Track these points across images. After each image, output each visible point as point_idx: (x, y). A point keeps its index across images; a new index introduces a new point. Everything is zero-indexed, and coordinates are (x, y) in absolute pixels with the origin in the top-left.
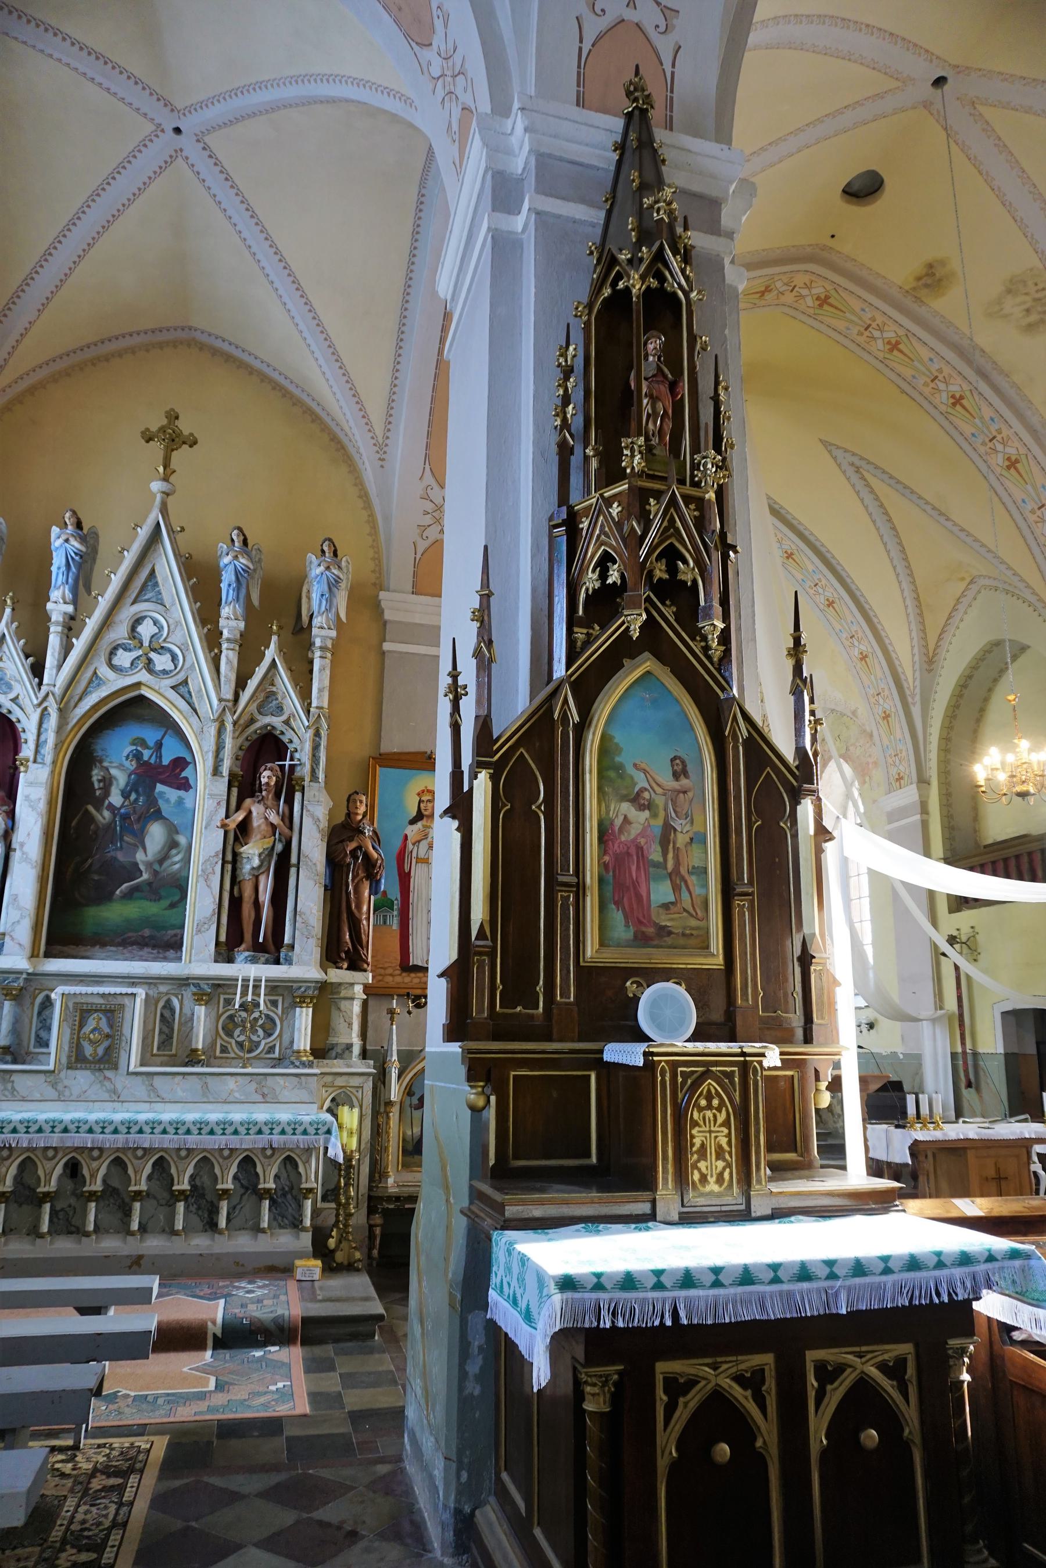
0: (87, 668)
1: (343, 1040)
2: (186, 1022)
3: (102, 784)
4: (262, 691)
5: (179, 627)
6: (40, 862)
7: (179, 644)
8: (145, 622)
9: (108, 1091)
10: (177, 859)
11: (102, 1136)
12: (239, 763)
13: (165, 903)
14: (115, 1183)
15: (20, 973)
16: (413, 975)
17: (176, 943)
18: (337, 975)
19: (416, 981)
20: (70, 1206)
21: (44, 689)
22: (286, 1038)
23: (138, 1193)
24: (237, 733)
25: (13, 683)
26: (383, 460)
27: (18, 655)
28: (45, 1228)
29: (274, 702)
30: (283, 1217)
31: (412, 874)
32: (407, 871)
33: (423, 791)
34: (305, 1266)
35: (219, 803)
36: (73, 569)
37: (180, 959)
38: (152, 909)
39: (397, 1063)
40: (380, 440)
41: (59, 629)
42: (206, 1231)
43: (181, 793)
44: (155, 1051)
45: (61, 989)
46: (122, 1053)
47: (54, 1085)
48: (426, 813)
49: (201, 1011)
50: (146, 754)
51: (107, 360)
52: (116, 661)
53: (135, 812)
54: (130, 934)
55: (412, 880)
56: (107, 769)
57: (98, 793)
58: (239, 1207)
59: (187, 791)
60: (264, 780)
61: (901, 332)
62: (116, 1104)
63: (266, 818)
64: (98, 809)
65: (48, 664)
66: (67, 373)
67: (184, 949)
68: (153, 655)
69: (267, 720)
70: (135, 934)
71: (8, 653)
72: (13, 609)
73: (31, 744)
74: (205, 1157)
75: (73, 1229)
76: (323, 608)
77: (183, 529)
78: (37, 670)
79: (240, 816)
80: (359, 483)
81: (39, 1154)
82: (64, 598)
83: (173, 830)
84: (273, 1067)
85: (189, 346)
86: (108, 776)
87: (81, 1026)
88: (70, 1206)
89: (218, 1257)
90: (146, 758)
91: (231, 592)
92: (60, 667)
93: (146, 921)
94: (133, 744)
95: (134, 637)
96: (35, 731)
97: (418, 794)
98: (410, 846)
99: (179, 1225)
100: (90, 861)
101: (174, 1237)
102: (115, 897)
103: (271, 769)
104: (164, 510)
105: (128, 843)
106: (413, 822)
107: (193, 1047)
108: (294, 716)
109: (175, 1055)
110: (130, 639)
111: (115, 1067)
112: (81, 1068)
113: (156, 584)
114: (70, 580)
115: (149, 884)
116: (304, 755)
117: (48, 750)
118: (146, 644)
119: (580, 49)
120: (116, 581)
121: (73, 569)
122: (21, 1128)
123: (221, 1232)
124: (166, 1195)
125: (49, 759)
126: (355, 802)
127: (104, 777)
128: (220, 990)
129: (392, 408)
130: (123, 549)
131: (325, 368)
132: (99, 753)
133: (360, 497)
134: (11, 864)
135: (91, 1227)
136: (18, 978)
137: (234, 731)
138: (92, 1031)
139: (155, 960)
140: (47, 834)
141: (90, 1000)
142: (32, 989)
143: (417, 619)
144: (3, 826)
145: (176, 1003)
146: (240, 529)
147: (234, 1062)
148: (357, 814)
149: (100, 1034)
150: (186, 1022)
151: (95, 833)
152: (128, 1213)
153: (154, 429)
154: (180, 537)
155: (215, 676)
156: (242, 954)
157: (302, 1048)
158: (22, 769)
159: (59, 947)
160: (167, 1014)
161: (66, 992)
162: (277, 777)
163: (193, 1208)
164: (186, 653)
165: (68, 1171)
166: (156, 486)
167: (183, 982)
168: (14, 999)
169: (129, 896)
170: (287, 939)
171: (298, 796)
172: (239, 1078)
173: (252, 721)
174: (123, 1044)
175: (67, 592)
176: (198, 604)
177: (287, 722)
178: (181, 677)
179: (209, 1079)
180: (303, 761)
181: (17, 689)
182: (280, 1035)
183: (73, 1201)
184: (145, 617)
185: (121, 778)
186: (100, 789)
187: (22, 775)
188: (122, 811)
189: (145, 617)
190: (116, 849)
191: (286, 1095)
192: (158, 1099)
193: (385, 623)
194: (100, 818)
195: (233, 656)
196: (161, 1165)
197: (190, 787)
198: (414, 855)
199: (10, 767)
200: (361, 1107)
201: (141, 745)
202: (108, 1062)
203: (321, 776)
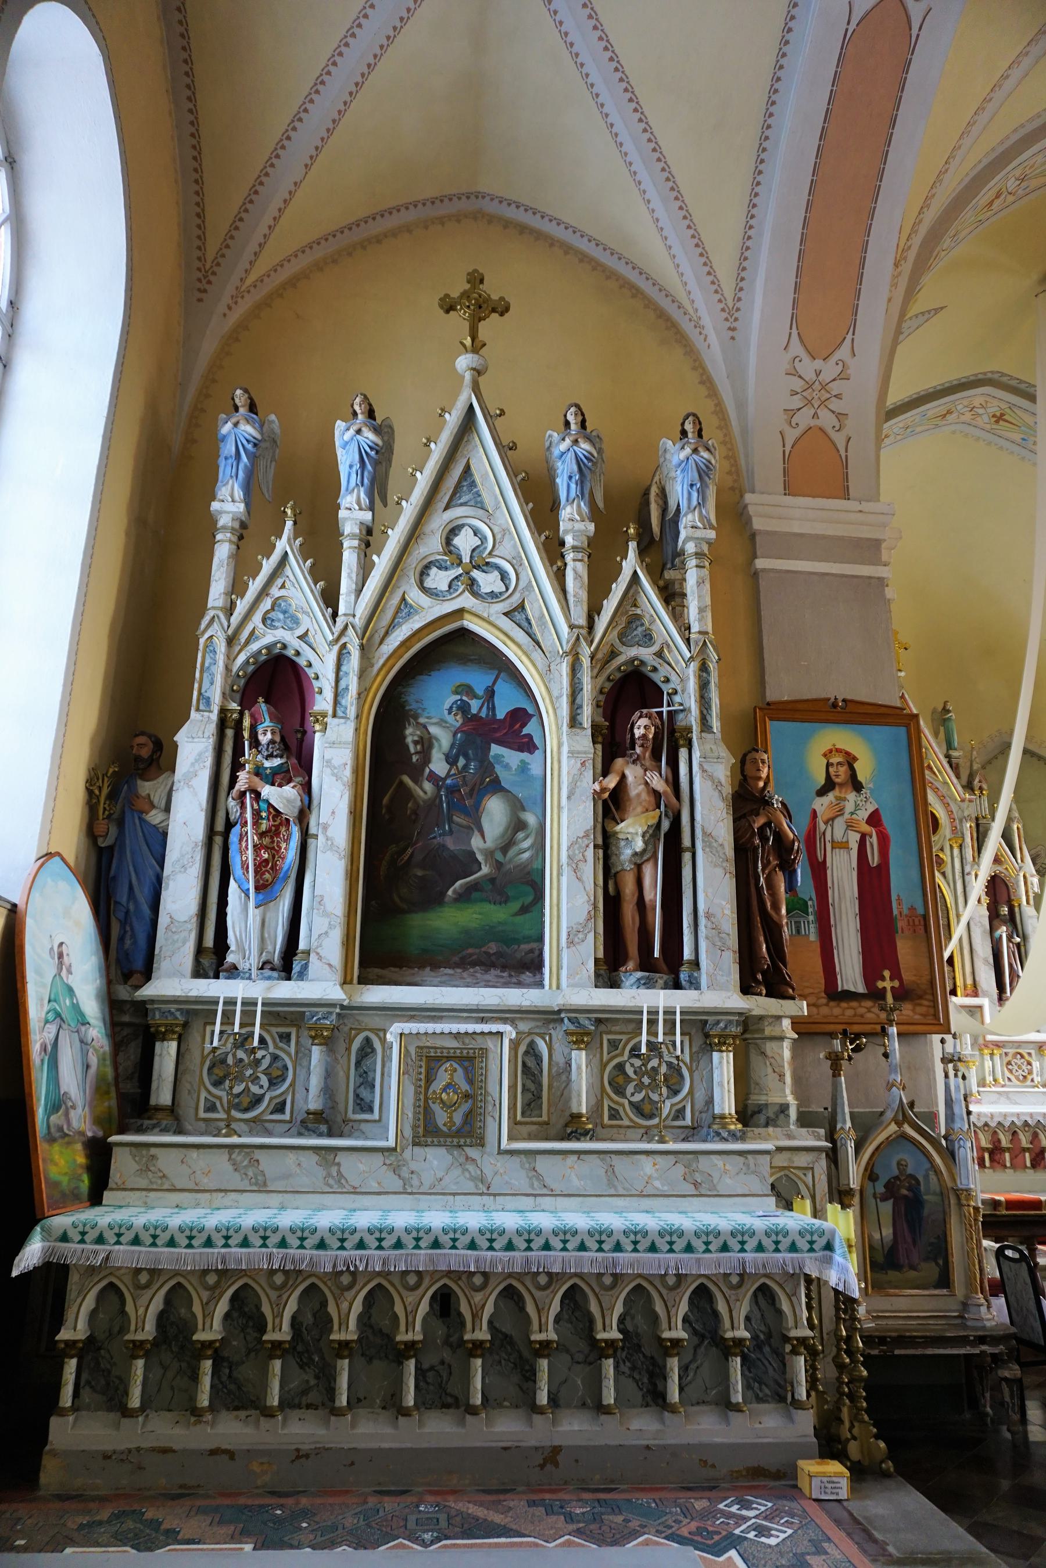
0: (391, 593)
1: (775, 1099)
2: (559, 1074)
3: (419, 747)
4: (622, 614)
5: (507, 536)
6: (348, 852)
7: (509, 558)
8: (463, 531)
9: (472, 1179)
10: (526, 844)
11: (490, 1253)
12: (600, 710)
13: (515, 906)
14: (507, 1327)
15: (333, 1005)
16: (844, 1005)
17: (532, 961)
18: (760, 1005)
19: (849, 1013)
20: (442, 1363)
21: (341, 621)
22: (700, 1095)
23: (546, 1344)
24: (596, 671)
25: (299, 615)
26: (733, 329)
27: (305, 578)
28: (410, 1400)
29: (640, 629)
30: (760, 1383)
31: (829, 864)
32: (820, 859)
33: (831, 751)
34: (824, 1474)
35: (583, 764)
36: (369, 467)
37: (540, 985)
38: (498, 914)
39: (852, 1132)
40: (730, 304)
41: (356, 543)
42: (647, 1405)
43: (524, 756)
44: (519, 1117)
45: (395, 1030)
46: (489, 1119)
47: (396, 1170)
48: (837, 780)
49: (580, 1058)
50: (475, 705)
51: (379, 242)
52: (429, 583)
53: (465, 784)
54: (470, 951)
55: (829, 872)
56: (425, 727)
57: (415, 758)
58: (693, 1366)
59: (531, 753)
60: (638, 733)
61: (1004, 406)
62: (485, 1198)
63: (647, 783)
64: (417, 781)
65: (343, 589)
66: (334, 260)
67: (546, 970)
68: (476, 574)
69: (633, 652)
70: (477, 951)
71: (292, 577)
72: (295, 523)
73: (329, 694)
74: (639, 1286)
75: (450, 1400)
76: (694, 502)
77: (502, 413)
78: (330, 599)
79: (611, 782)
80: (699, 365)
81: (396, 1281)
82: (358, 503)
83: (517, 806)
84: (685, 1140)
85: (475, 219)
86: (426, 736)
87: (429, 1080)
88: (442, 1363)
89: (674, 1452)
90: (474, 711)
91: (573, 486)
92: (359, 591)
93: (491, 933)
94: (456, 693)
95: (450, 552)
96: (331, 676)
97: (825, 755)
98: (822, 826)
99: (609, 1397)
100: (410, 851)
101: (603, 1417)
102: (447, 899)
103: (649, 716)
104: (476, 389)
105: (458, 824)
106: (822, 792)
107: (575, 1111)
108: (668, 646)
109: (547, 1123)
110: (445, 554)
111: (481, 1143)
112: (432, 1145)
113: (473, 484)
114: (366, 481)
115: (491, 880)
116: (690, 698)
117: (350, 700)
118: (466, 559)
119: (784, 452)
120: (423, 480)
121: (369, 467)
122: (371, 1241)
123: (672, 1409)
124: (583, 1345)
125: (352, 712)
126: (755, 761)
127: (422, 738)
128: (602, 1027)
129: (746, 259)
130: (429, 440)
131: (660, 213)
132: (413, 706)
133: (702, 382)
134: (311, 855)
135: (477, 1400)
136: (331, 1013)
137: (592, 668)
138: (444, 1090)
139: (506, 985)
140: (354, 813)
141: (439, 1043)
142: (346, 1029)
143: (796, 528)
144: (299, 803)
145: (542, 1046)
146: (577, 406)
147: (630, 1133)
148: (760, 778)
149: (455, 1092)
150: (559, 1074)
151: (415, 813)
152: (530, 1376)
153: (455, 294)
154: (499, 422)
155: (561, 596)
156: (631, 975)
157: (727, 1112)
158: (317, 727)
159: (377, 970)
160: (531, 1063)
161: (406, 1032)
162: (656, 727)
163: (625, 1368)
164: (520, 570)
165: (437, 1307)
166: (464, 362)
167: (550, 1017)
168: (325, 1044)
169: (465, 897)
170: (687, 954)
171: (683, 753)
172: (659, 1159)
173: (613, 654)
174: (490, 1108)
175: (362, 495)
176: (531, 505)
177: (660, 654)
178: (515, 600)
179: (616, 1160)
180: (686, 705)
181: (306, 623)
182: (691, 1092)
183: (446, 1354)
184: (463, 525)
185: (443, 738)
186: (416, 753)
187: (317, 735)
188: (449, 781)
189: (463, 525)
190: (444, 834)
191: (728, 1184)
192: (545, 1191)
193: (753, 536)
194: (421, 793)
195: (582, 568)
196: (574, 1299)
197: (536, 748)
198: (828, 837)
199: (297, 731)
200: (813, 1198)
201: (467, 695)
202: (470, 1134)
203: (715, 724)
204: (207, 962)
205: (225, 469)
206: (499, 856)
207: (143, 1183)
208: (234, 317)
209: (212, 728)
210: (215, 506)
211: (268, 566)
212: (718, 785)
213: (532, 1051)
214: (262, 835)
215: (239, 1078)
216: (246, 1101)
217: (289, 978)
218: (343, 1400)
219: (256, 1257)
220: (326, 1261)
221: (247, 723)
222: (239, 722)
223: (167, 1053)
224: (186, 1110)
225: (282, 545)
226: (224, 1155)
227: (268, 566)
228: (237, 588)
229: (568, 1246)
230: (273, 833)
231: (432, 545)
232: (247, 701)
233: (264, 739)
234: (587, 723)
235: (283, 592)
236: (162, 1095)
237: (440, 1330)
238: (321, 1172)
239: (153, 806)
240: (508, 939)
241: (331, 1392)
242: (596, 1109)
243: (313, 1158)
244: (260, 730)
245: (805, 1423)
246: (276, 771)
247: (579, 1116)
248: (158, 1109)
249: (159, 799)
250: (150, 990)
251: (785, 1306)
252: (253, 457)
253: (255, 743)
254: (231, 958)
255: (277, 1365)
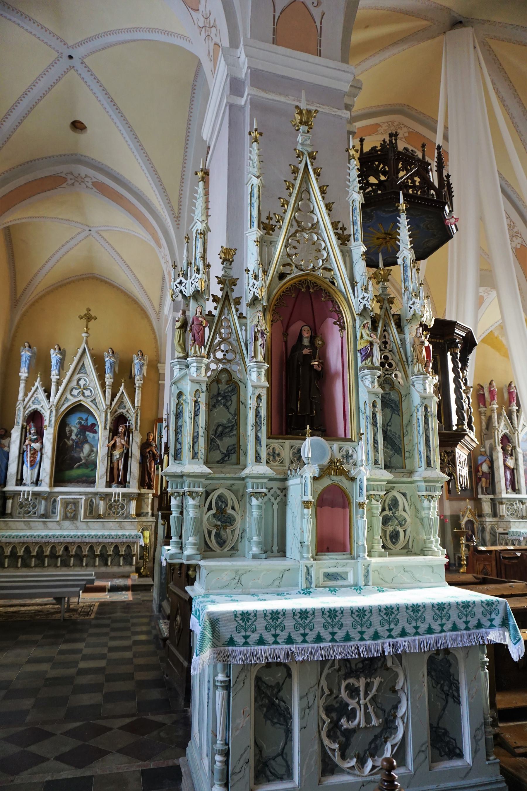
1: (146, 511)
13: (90, 469)
14: (78, 553)
21: (51, 403)
22: (128, 510)
37: (94, 487)
41: (55, 384)
43: (94, 434)
47: (59, 525)
49: (102, 503)
50: (83, 422)
52: (73, 393)
60: (120, 430)
68: (84, 391)
78: (48, 397)
79: (113, 442)
80: (151, 325)
83: (92, 446)
87: (67, 507)
90: (83, 423)
92: (55, 396)
93: (84, 475)
104: (87, 343)
111: (77, 520)
113: (85, 367)
115: (85, 463)
116: (133, 422)
118: (82, 387)
120: (72, 367)
122: (52, 537)
125: (53, 425)
132: (68, 423)
145: (94, 500)
146: (111, 349)
153: (83, 315)
156: (114, 485)
160: (91, 504)
167: (96, 494)
169: (78, 467)
170: (128, 480)
171: (131, 435)
172: (114, 523)
173: (116, 411)
177: (127, 411)
178: (93, 398)
179: (105, 523)
181: (42, 404)
185: (75, 430)
191: (128, 527)
195: (110, 391)
203: (138, 428)
204: (19, 482)
205: (23, 364)
206: (87, 458)
207: (6, 528)
208: (25, 308)
209: (20, 430)
210: (20, 374)
211: (33, 389)
212: (137, 443)
213: (92, 501)
214: (32, 454)
215: (26, 507)
216: (27, 512)
217: (37, 486)
218: (46, 565)
219: (30, 540)
220: (43, 540)
221: (28, 428)
222: (26, 427)
223: (10, 502)
224: (14, 514)
225: (37, 384)
226: (22, 523)
227: (33, 389)
228: (26, 395)
229: (445, 628)
230: (34, 454)
231: (74, 384)
232: (28, 422)
233: (32, 432)
234: (108, 428)
235: (37, 396)
236: (9, 511)
237: (65, 553)
238: (43, 526)
239: (5, 446)
240: (88, 476)
241: (44, 564)
242: (105, 513)
243: (41, 523)
244: (31, 430)
245: (134, 568)
246: (35, 439)
247: (100, 515)
248: (8, 514)
249: (7, 444)
250: (6, 489)
251: (132, 548)
252: (30, 360)
253: (30, 434)
254: (24, 482)
255: (33, 560)
